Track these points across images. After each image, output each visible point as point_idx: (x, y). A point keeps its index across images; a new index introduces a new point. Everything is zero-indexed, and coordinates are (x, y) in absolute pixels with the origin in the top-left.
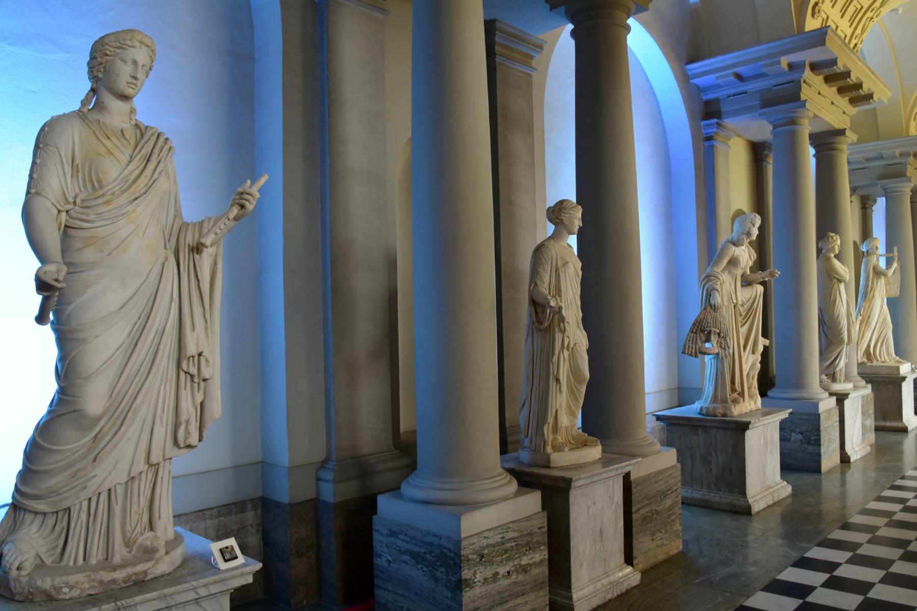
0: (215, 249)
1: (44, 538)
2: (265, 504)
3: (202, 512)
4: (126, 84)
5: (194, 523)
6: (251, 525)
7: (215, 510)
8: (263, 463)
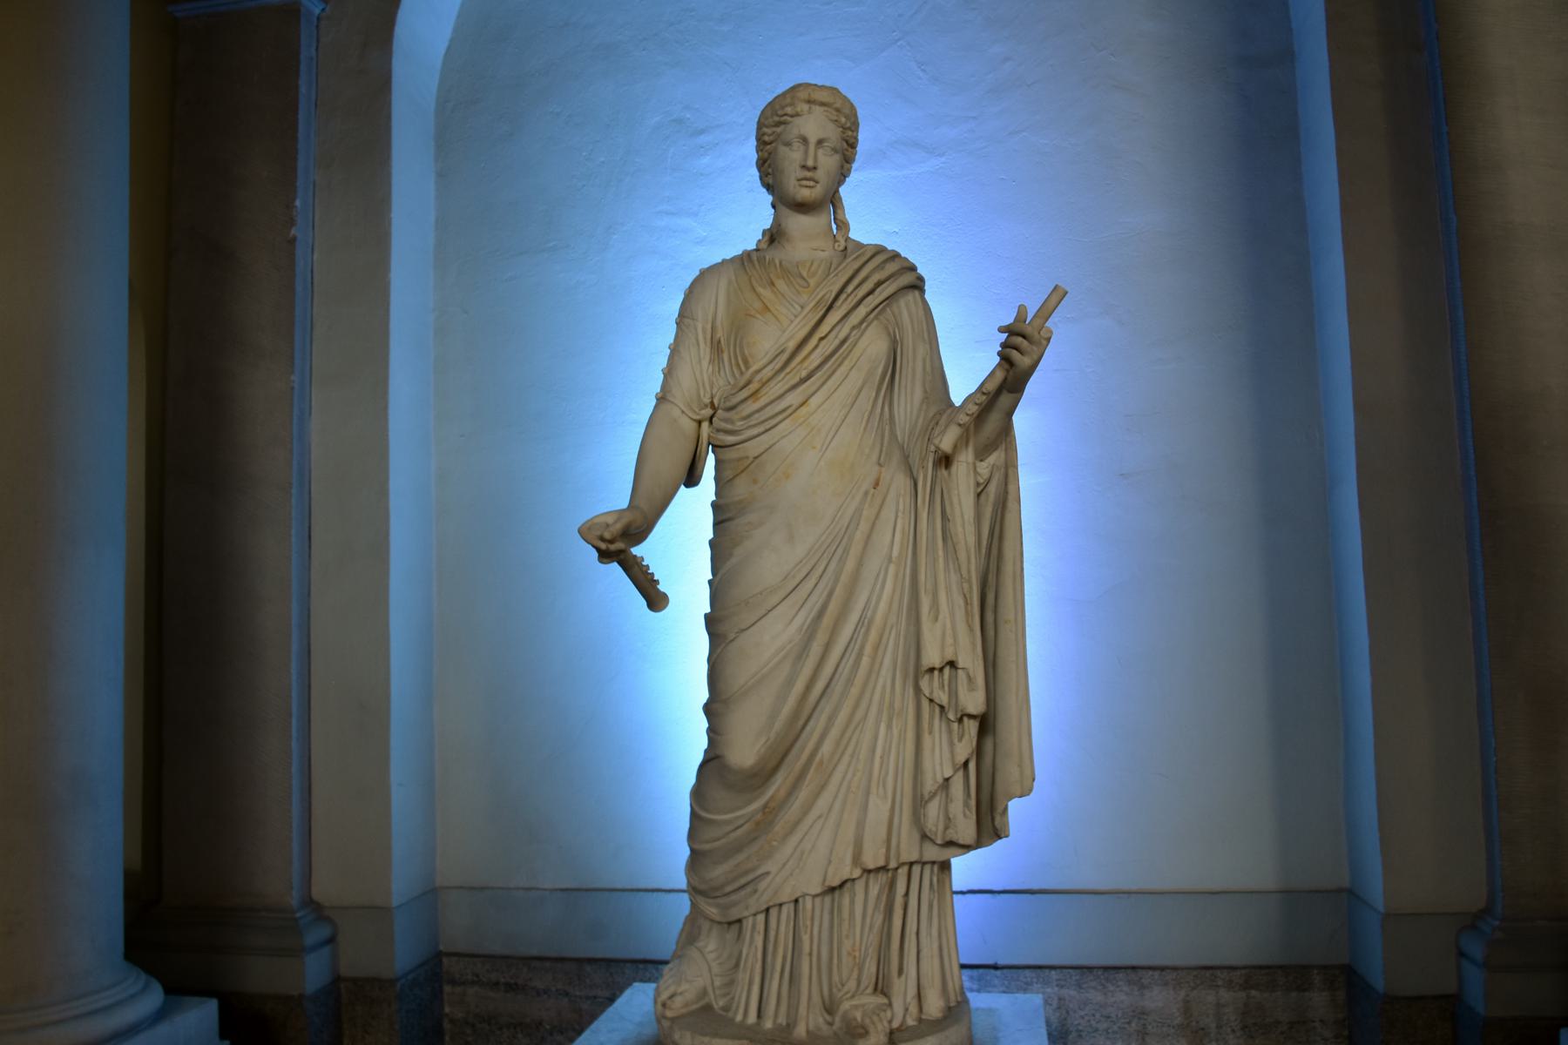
0: (1003, 455)
1: (720, 964)
2: (1347, 979)
3: (1211, 971)
4: (797, 183)
5: (1194, 989)
6: (1321, 1021)
7: (1238, 973)
8: (1351, 892)
